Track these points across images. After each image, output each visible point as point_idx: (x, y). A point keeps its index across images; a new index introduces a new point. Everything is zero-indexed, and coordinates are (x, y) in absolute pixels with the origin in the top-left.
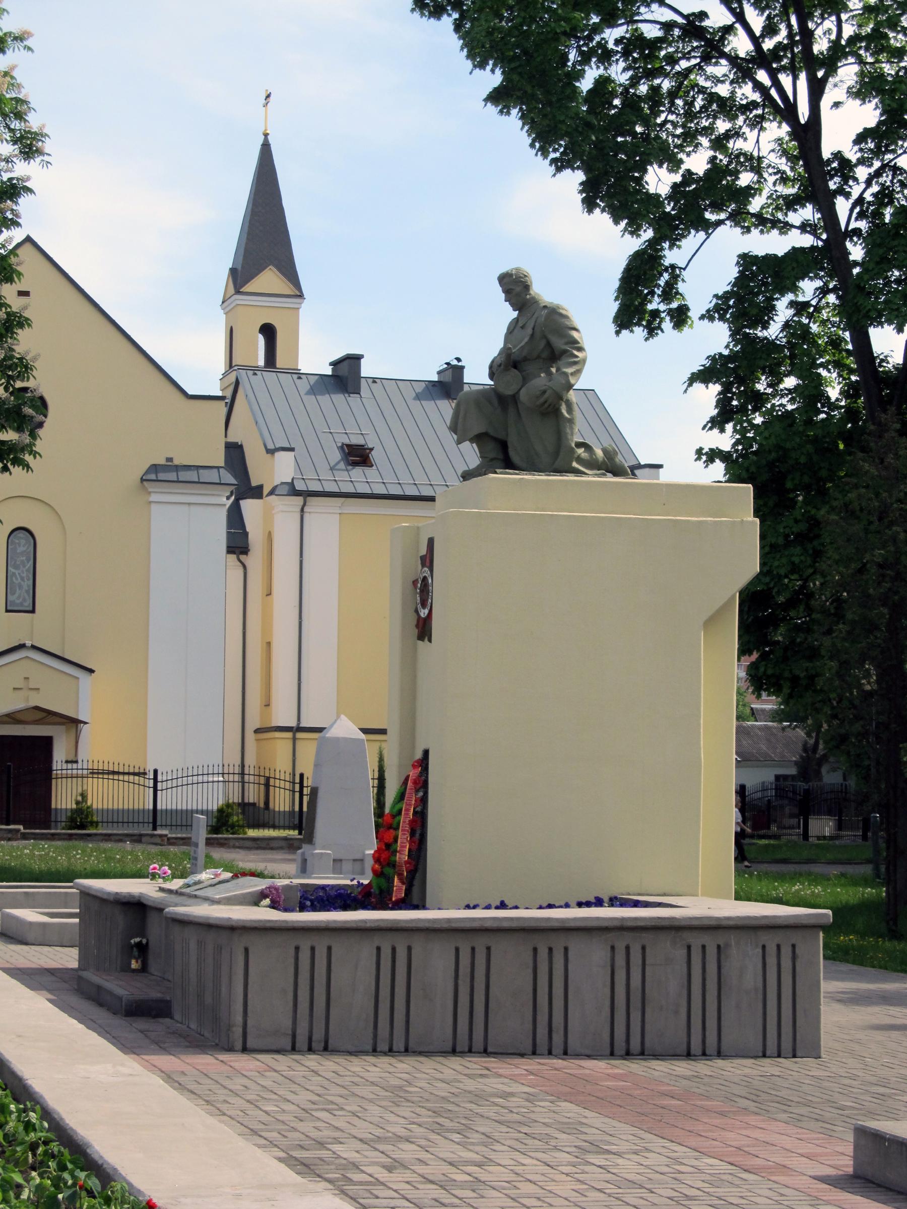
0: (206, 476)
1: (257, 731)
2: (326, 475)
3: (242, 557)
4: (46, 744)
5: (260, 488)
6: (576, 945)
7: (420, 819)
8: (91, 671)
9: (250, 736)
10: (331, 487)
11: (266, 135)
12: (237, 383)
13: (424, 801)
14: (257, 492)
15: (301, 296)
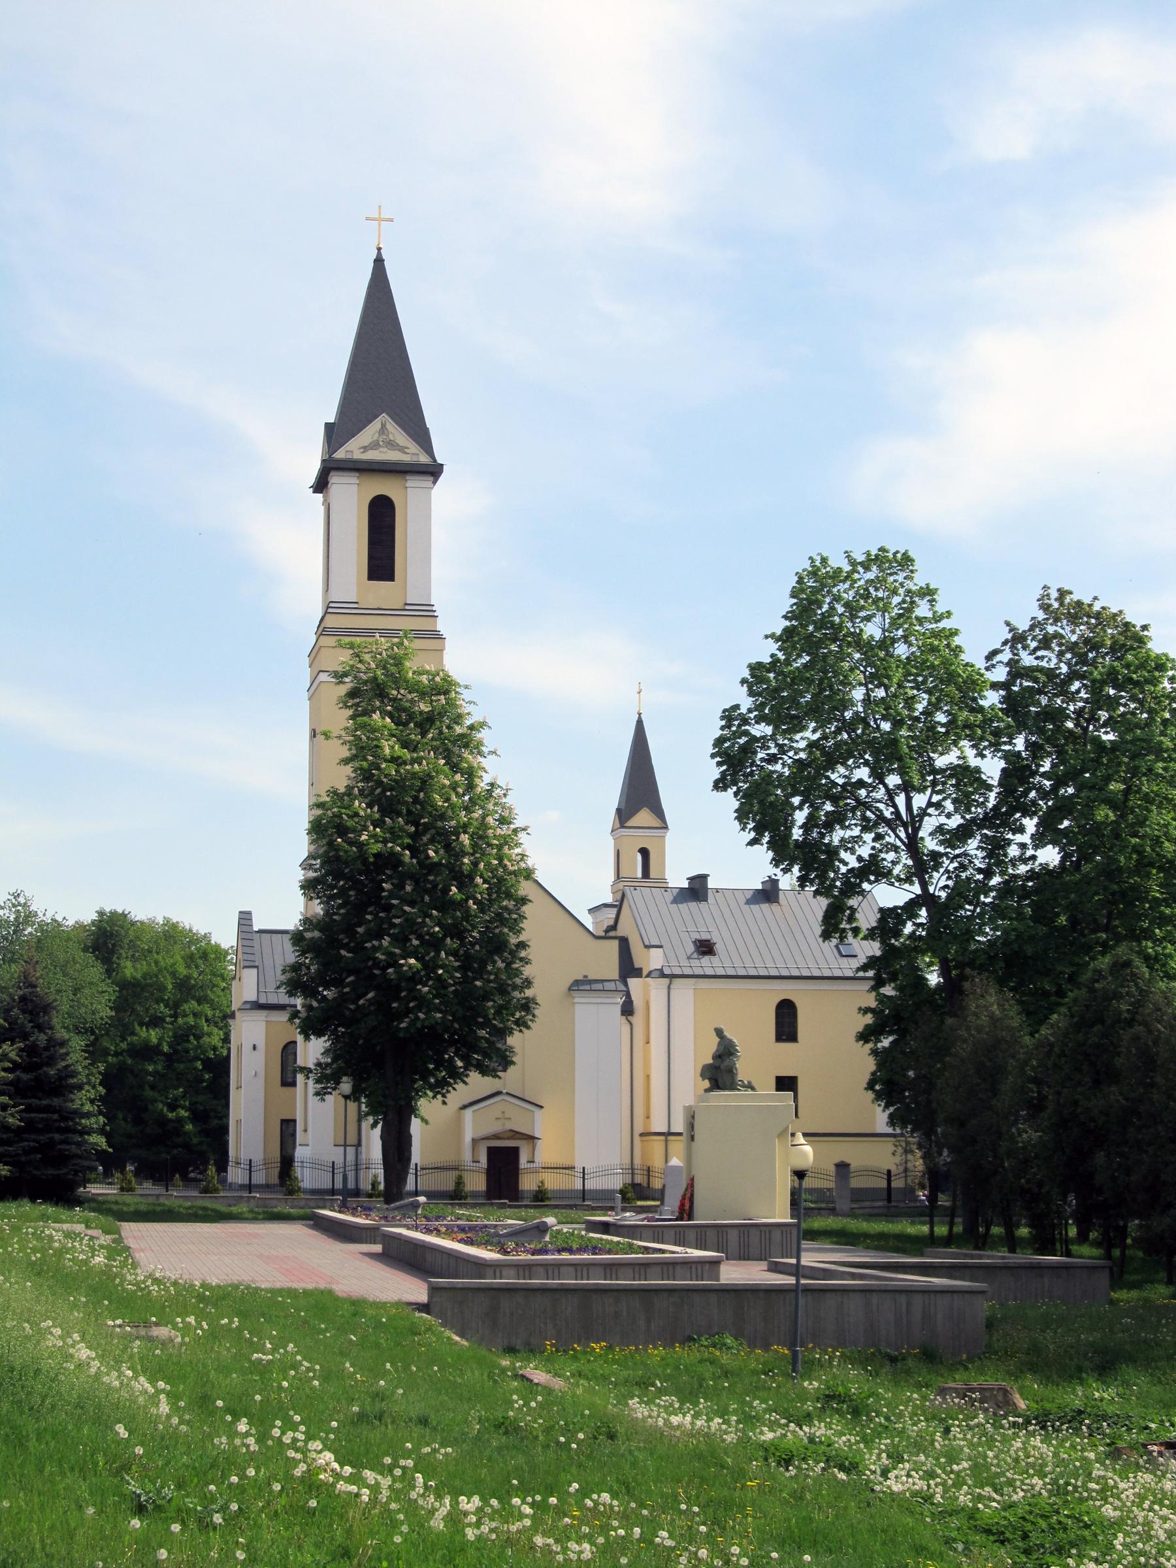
0: (609, 986)
1: (641, 1135)
2: (684, 963)
3: (629, 1018)
4: (515, 1152)
5: (640, 970)
6: (730, 1231)
7: (692, 1195)
8: (541, 1107)
9: (637, 1138)
10: (688, 971)
11: (640, 714)
12: (623, 896)
13: (693, 1191)
14: (638, 973)
15: (666, 828)
